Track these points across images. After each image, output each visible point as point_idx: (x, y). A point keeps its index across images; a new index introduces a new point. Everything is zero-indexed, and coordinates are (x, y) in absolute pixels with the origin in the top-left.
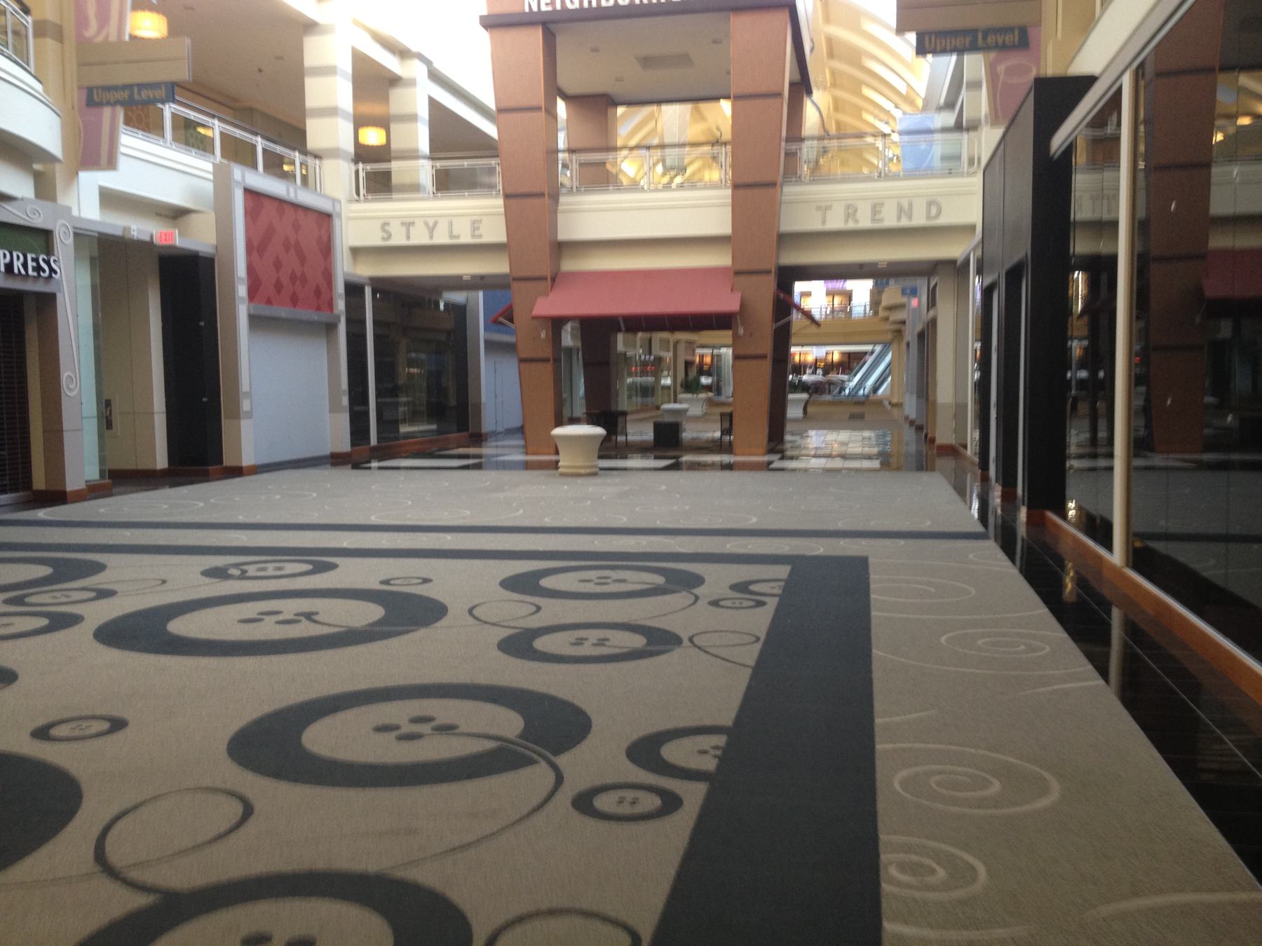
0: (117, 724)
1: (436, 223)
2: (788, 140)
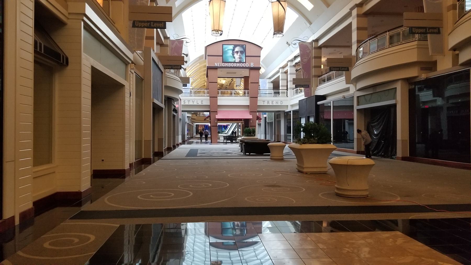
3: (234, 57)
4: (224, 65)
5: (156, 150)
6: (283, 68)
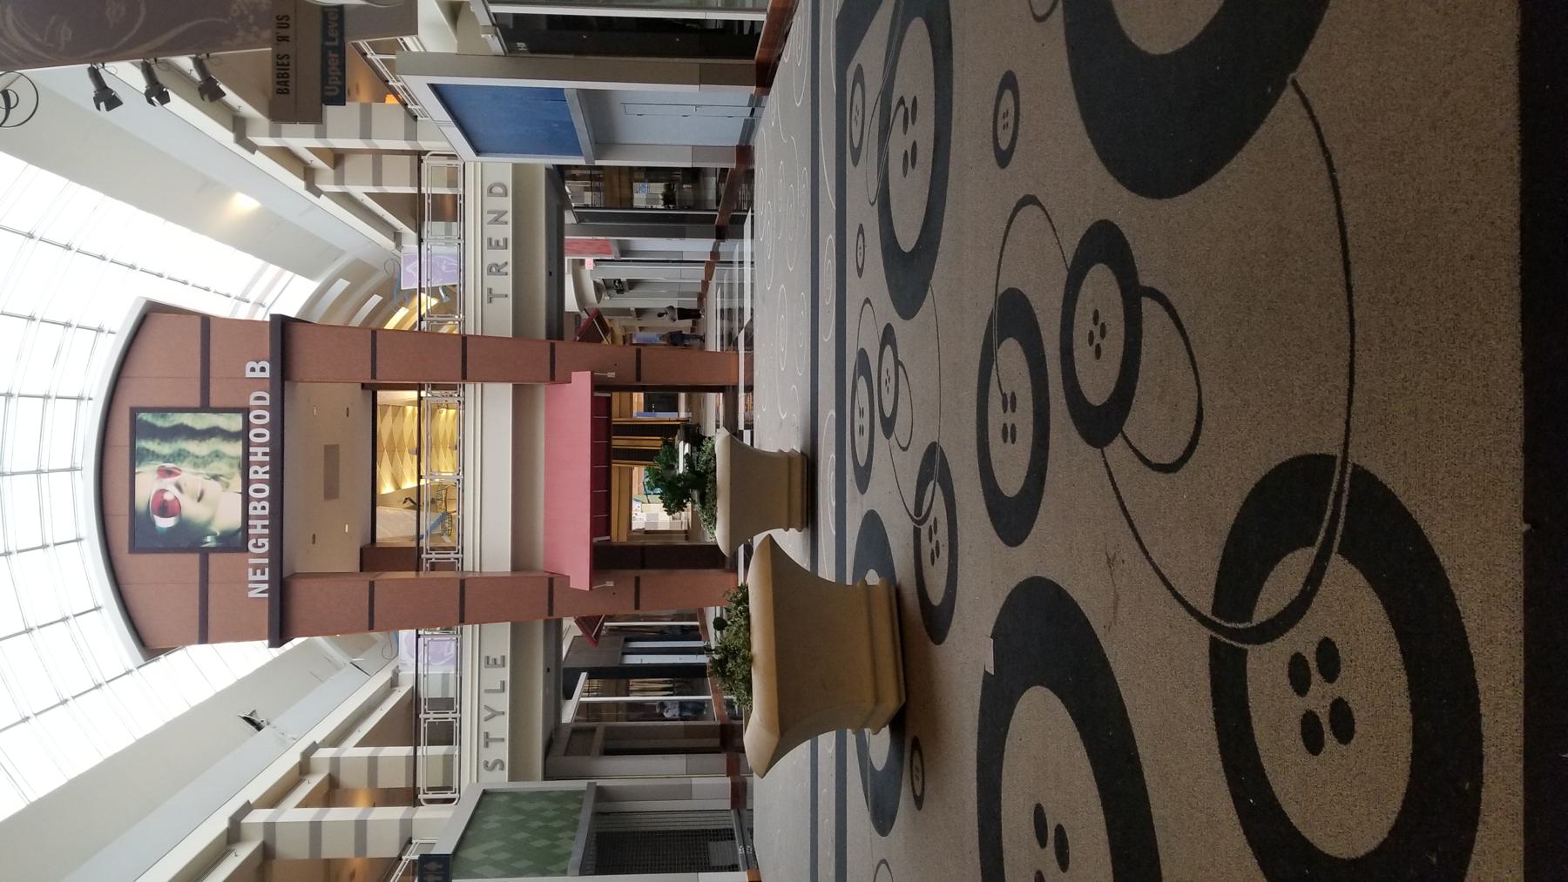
0: (1009, 82)
1: (487, 707)
2: (418, 569)
3: (206, 489)
4: (260, 546)
5: (716, 742)
6: (308, 174)
